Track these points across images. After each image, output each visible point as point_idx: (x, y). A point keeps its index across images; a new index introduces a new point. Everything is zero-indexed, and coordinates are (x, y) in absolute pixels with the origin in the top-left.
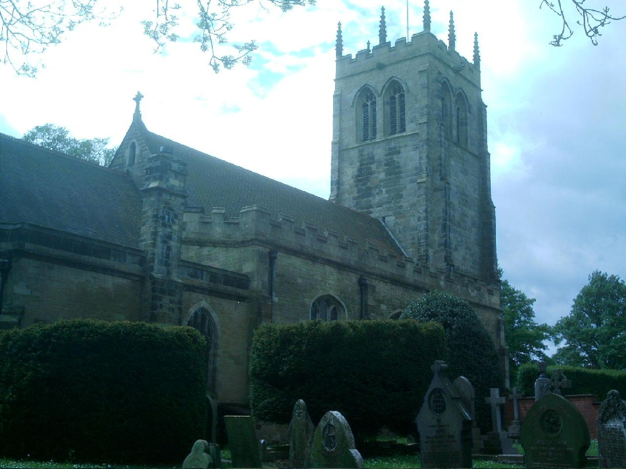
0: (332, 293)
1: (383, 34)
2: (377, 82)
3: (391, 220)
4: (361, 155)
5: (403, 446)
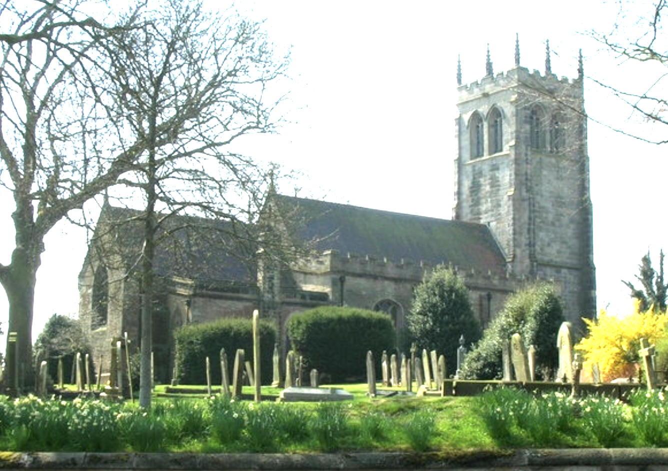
0: (390, 298)
3: (493, 225)
4: (474, 170)
5: (651, 365)
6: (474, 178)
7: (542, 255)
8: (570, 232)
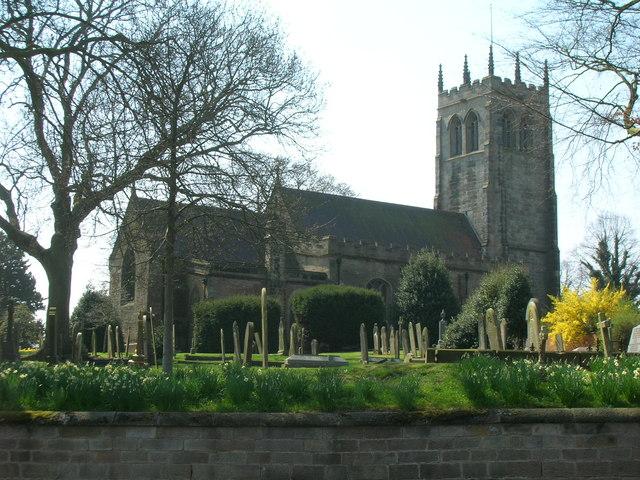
0: (381, 277)
1: (467, 75)
2: (462, 113)
3: (470, 214)
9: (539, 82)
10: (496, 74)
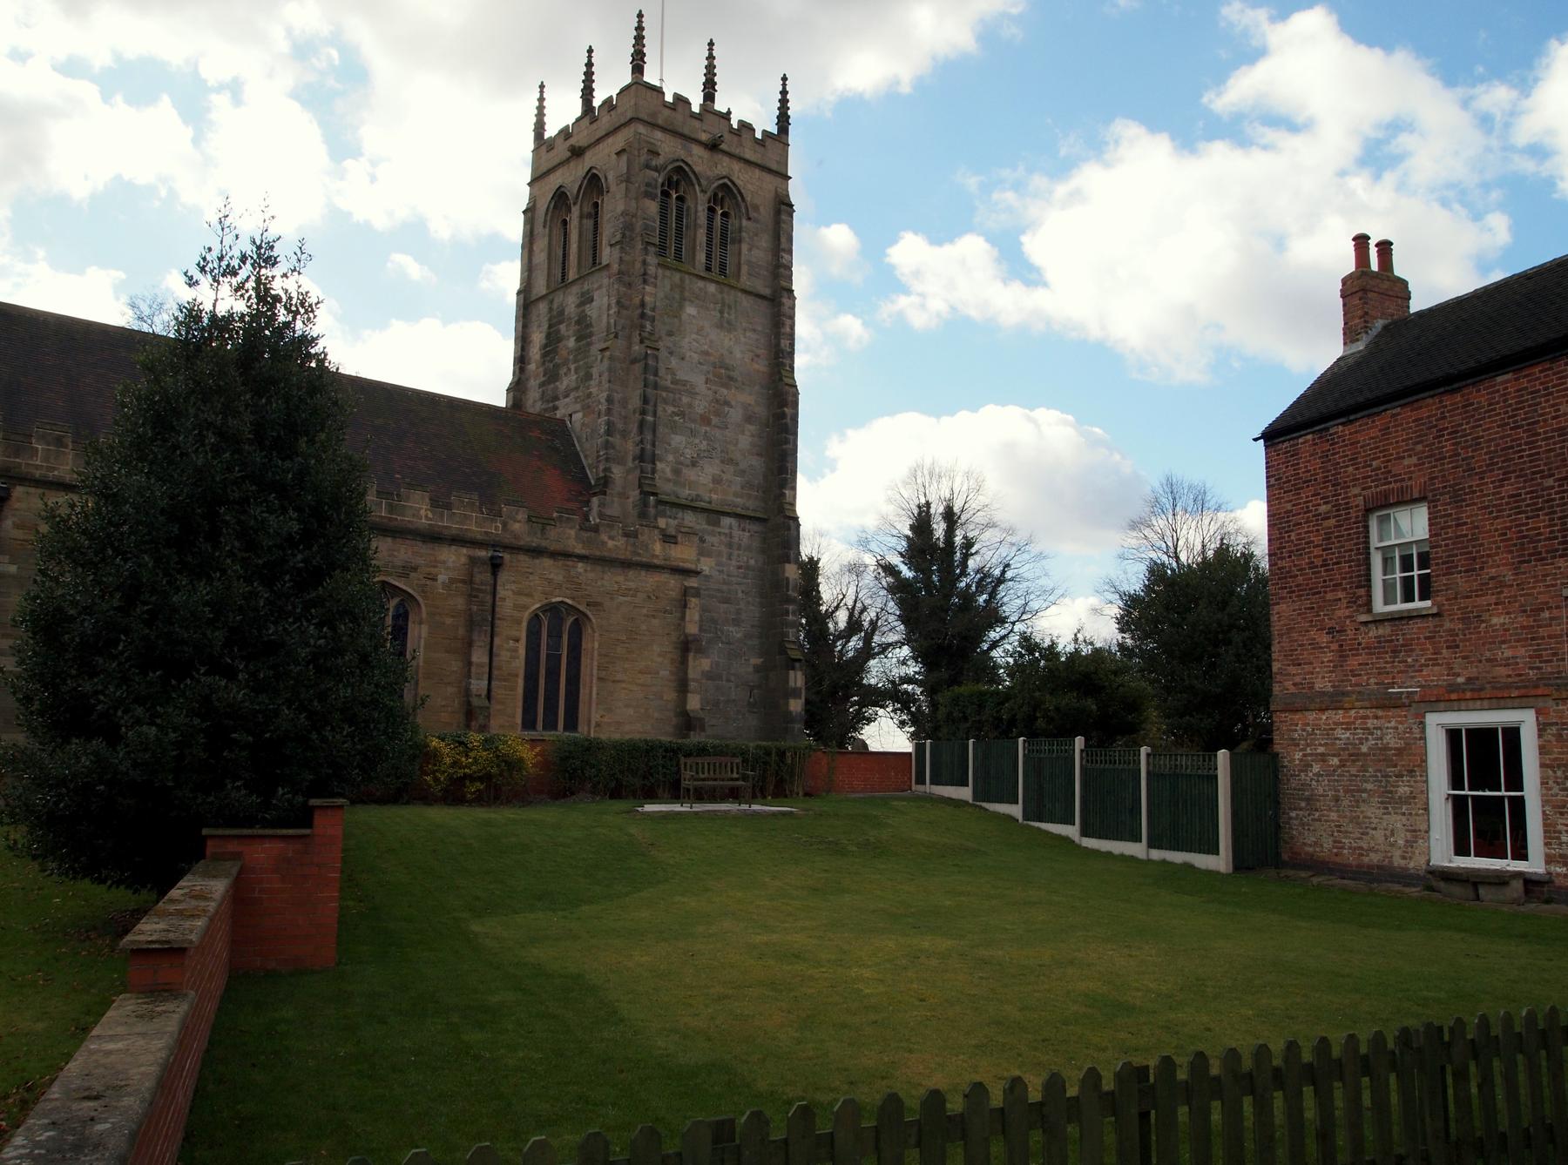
4: (551, 309)
6: (550, 327)
7: (676, 483)
8: (745, 440)
9: (764, 122)
10: (650, 77)
